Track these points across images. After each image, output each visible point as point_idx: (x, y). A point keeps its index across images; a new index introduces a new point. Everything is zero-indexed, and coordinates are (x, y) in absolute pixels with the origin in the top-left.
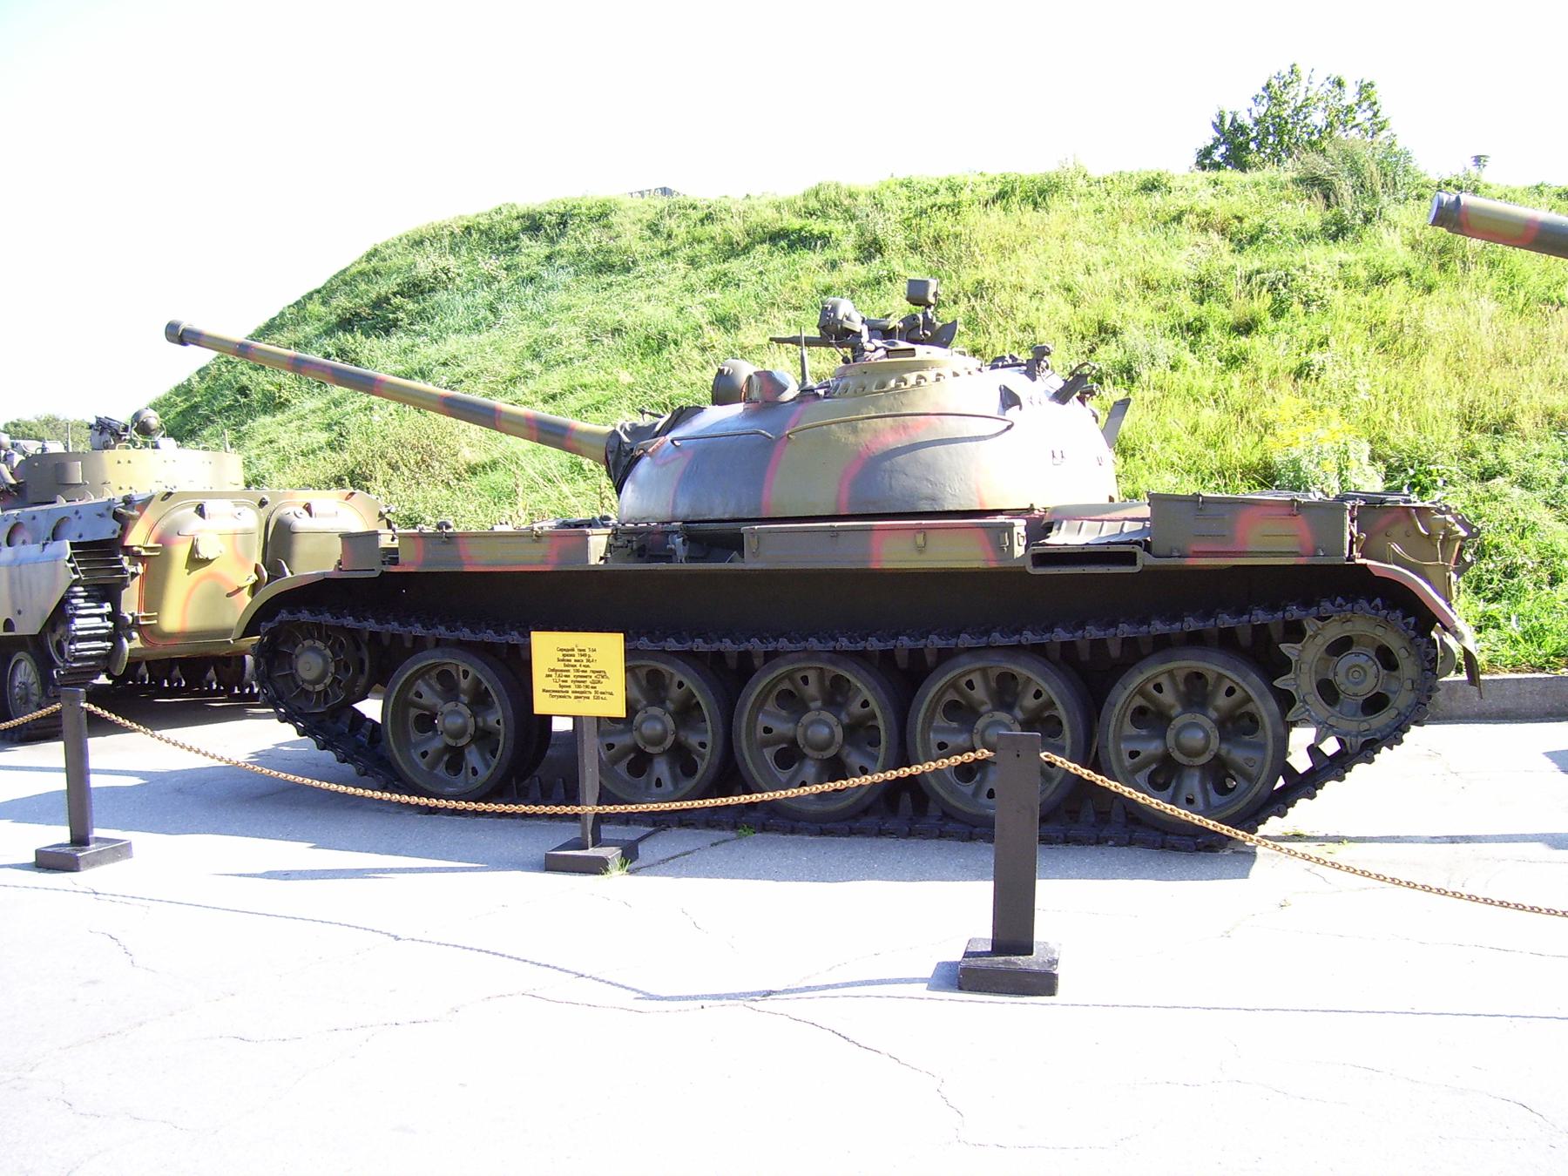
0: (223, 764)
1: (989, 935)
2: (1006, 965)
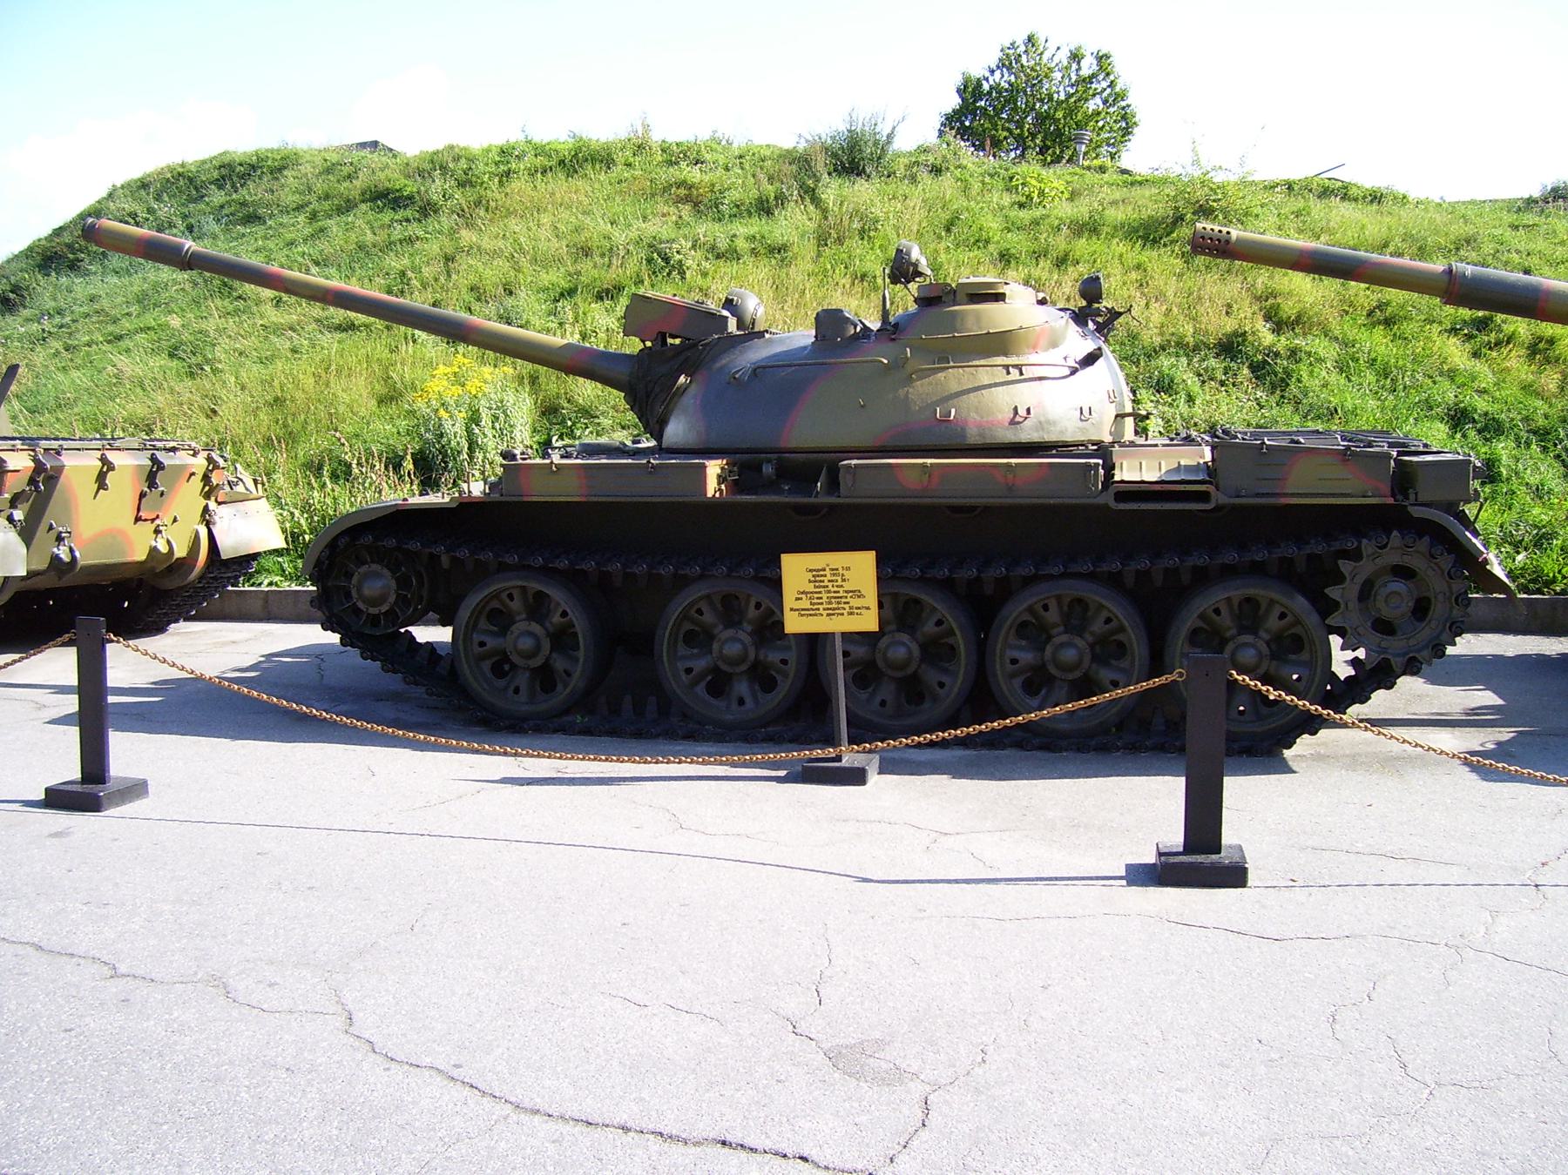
0: (185, 675)
1: (1182, 839)
2: (1201, 861)
